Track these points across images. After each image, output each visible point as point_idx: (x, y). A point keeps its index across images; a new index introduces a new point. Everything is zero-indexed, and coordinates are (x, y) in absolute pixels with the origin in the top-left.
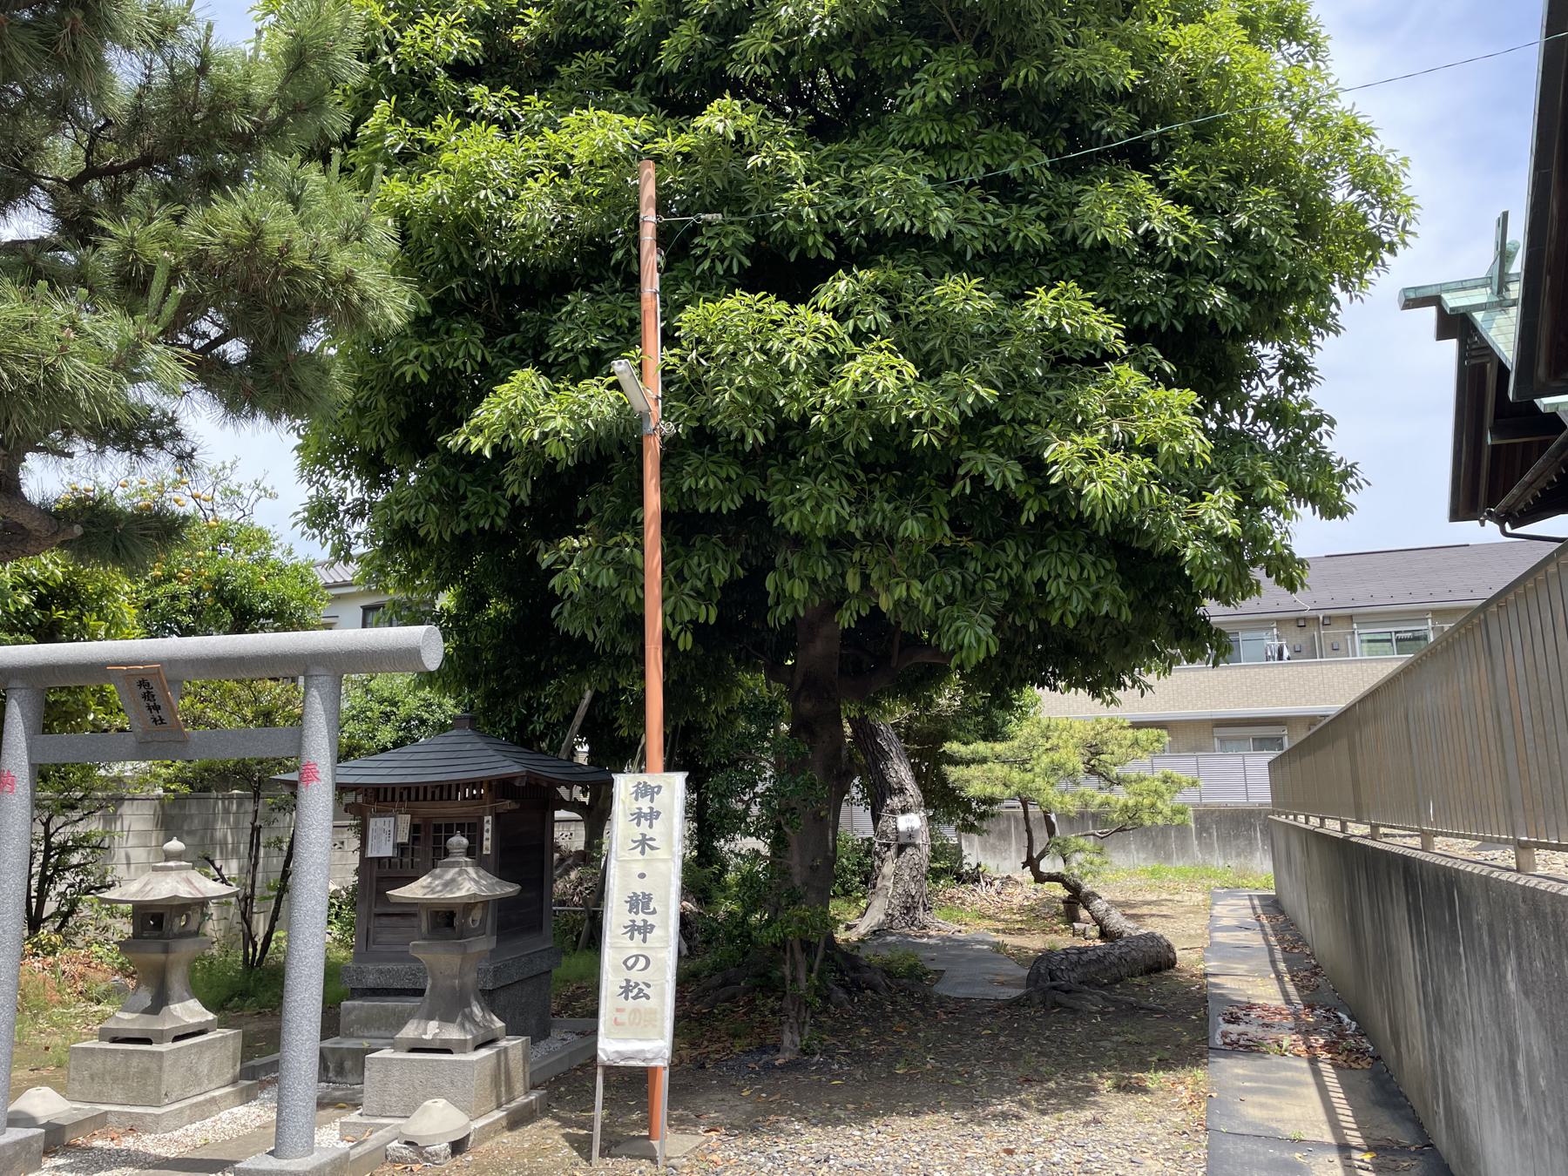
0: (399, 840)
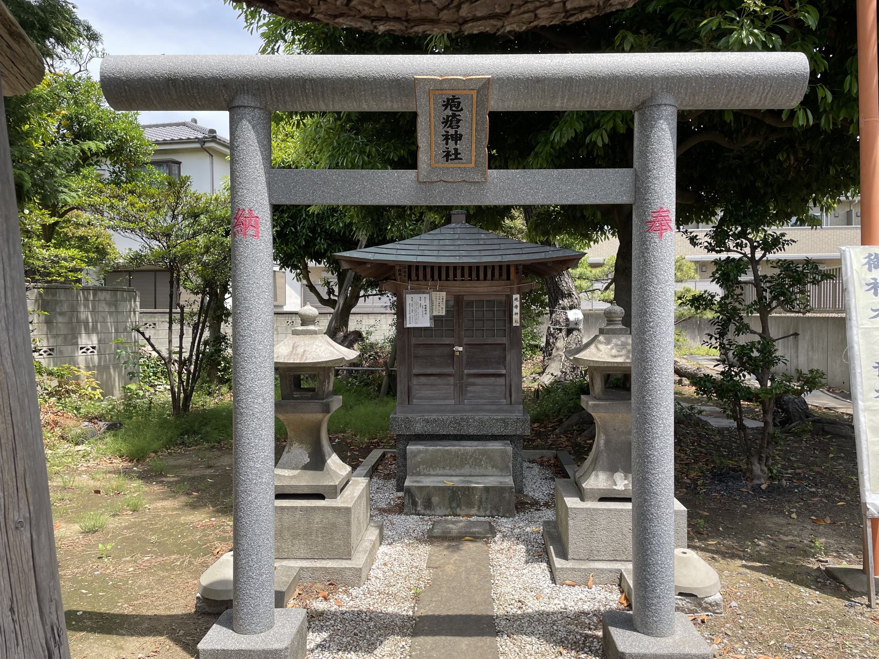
0: (435, 313)
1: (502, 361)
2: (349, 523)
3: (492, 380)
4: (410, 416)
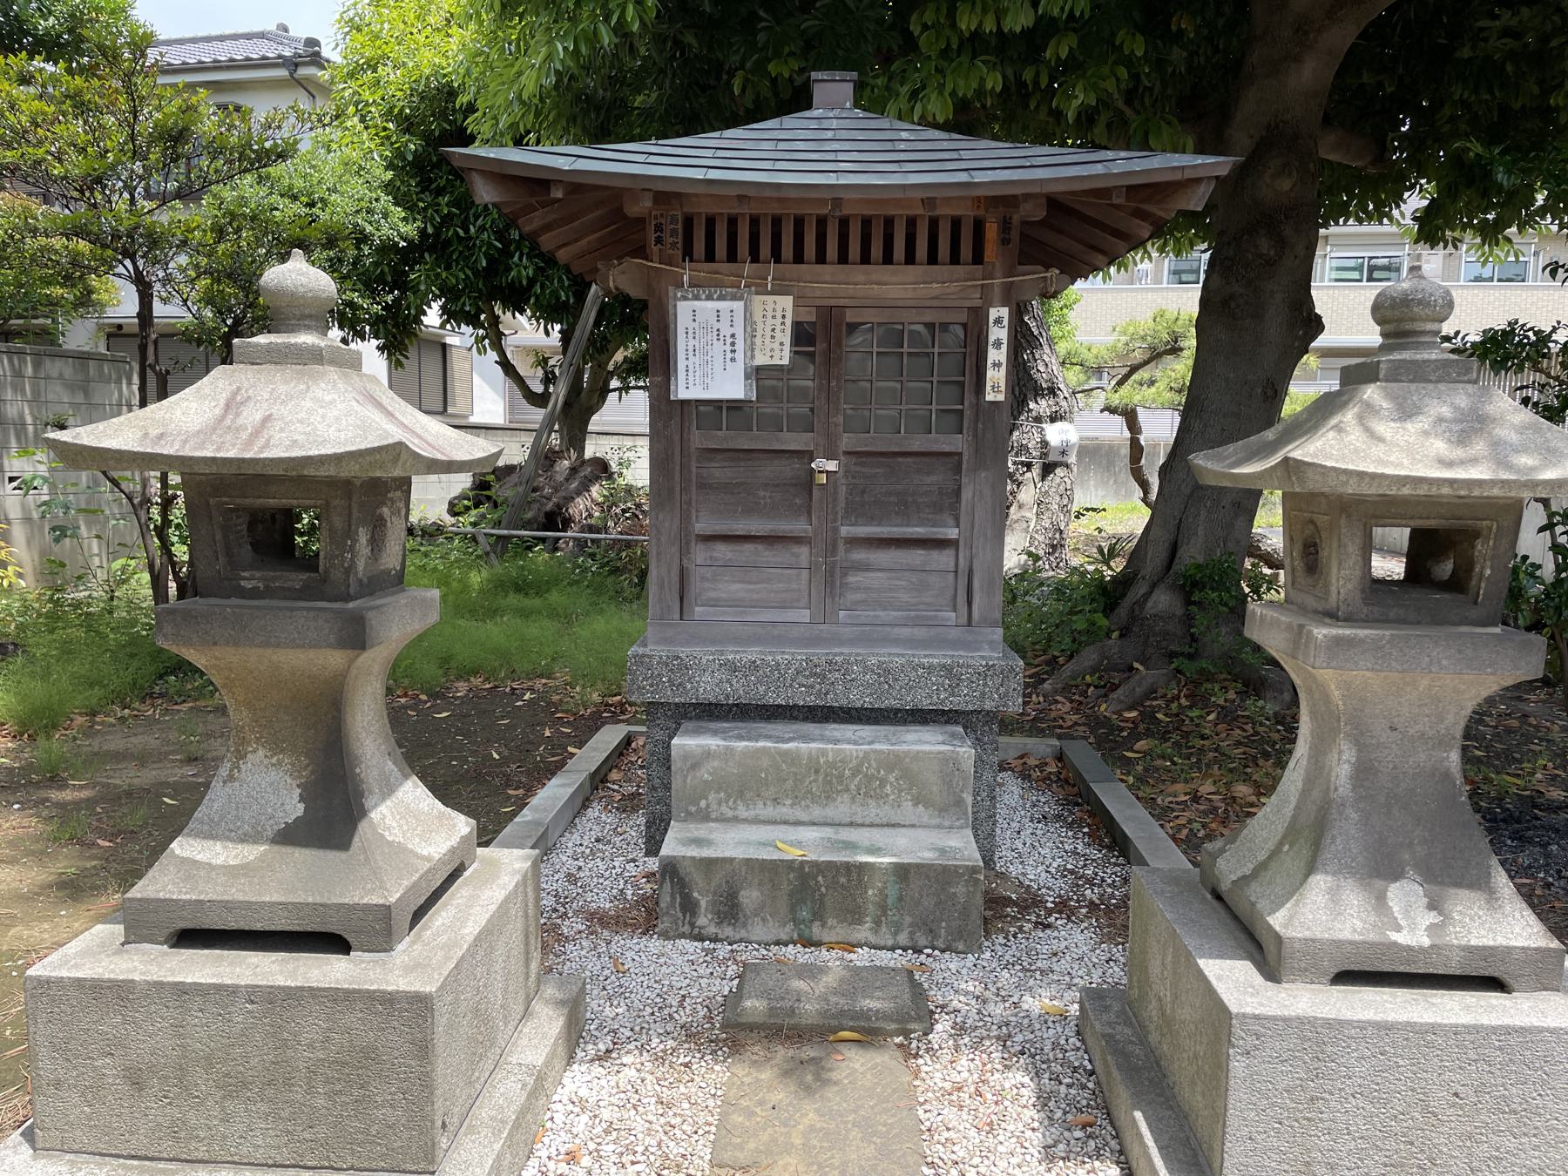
0: (761, 360)
1: (950, 501)
2: (424, 1050)
3: (917, 556)
4: (683, 651)
